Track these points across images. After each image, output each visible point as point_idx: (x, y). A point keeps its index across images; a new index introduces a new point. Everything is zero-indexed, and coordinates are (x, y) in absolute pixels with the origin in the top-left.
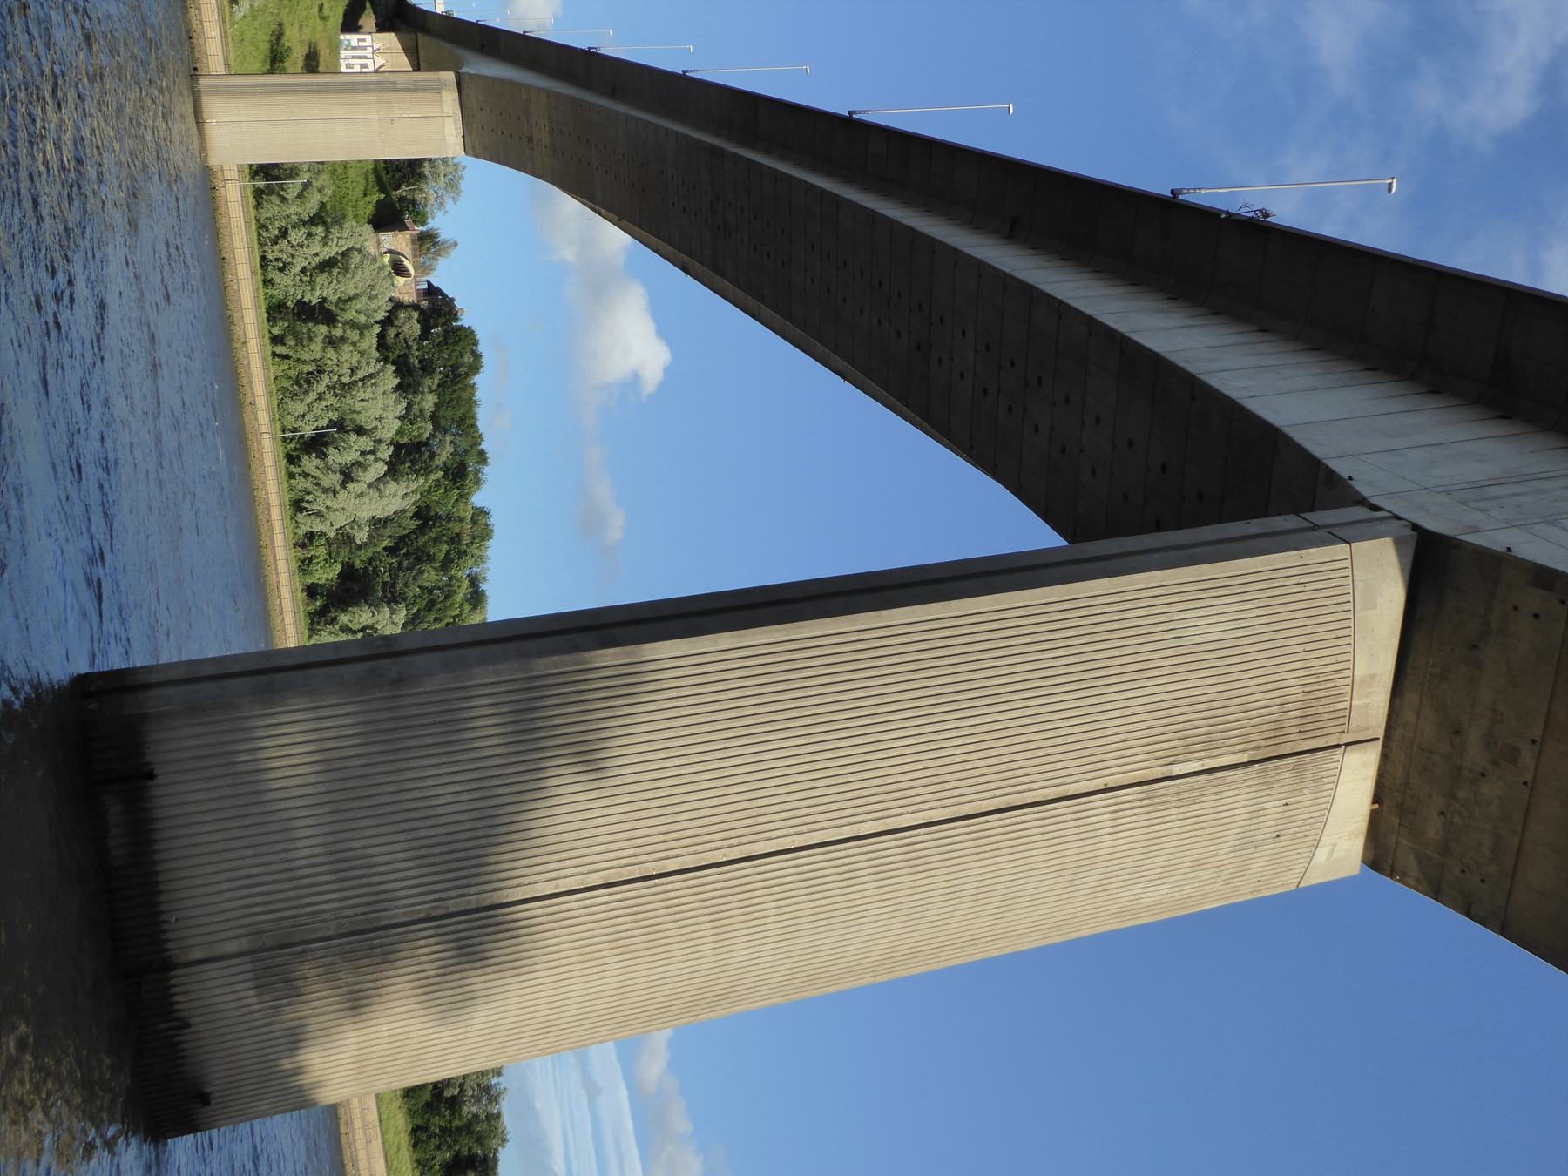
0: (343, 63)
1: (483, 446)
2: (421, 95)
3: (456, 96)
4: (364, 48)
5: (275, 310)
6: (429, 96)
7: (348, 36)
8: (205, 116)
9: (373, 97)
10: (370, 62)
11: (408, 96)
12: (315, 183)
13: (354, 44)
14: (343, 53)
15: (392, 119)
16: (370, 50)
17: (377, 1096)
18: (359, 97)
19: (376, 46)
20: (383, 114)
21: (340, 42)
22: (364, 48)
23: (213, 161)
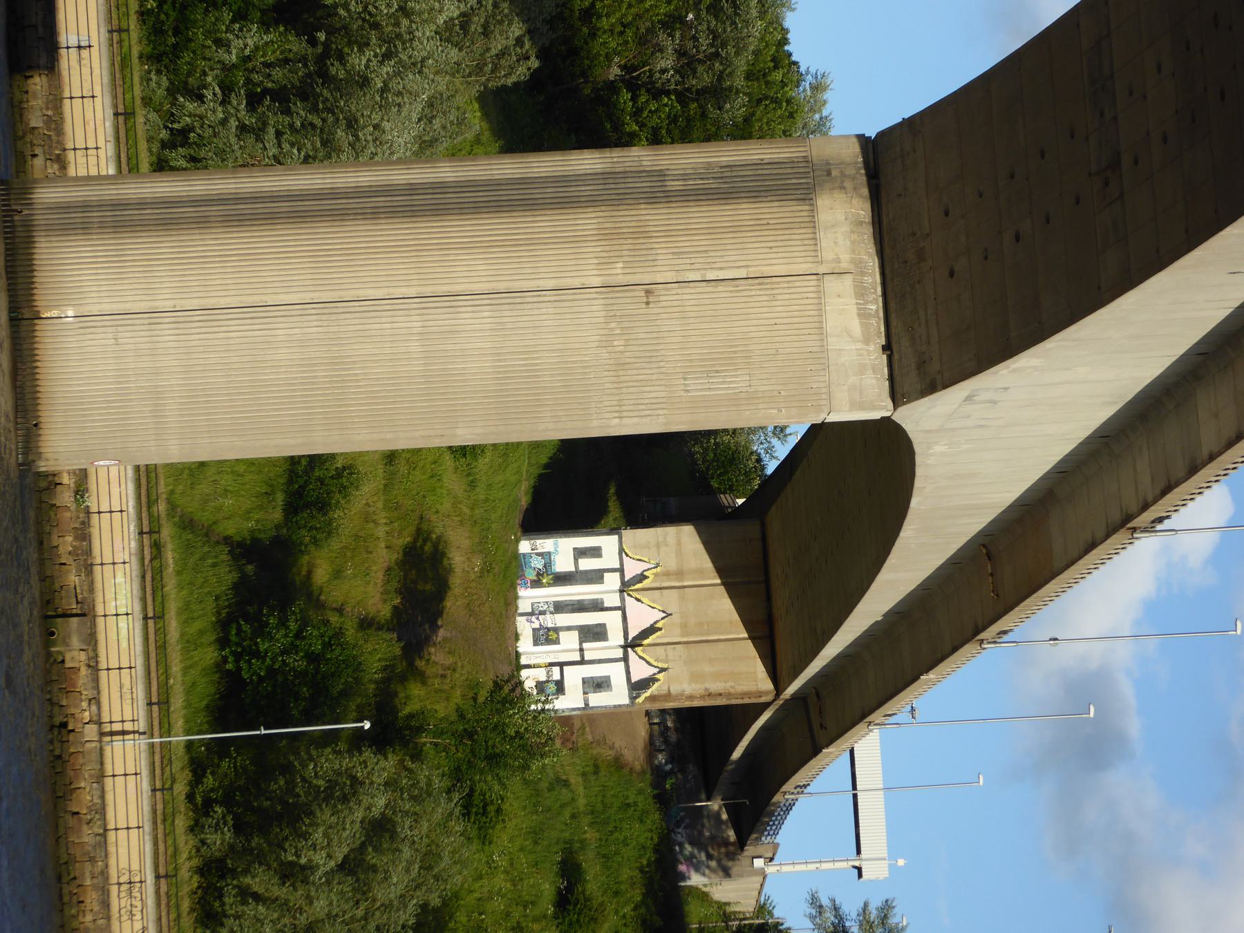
0: (525, 628)
1: (794, 58)
2: (745, 211)
3: (861, 208)
4: (596, 577)
5: (161, 166)
6: (771, 210)
7: (546, 544)
8: (42, 298)
9: (588, 221)
10: (612, 620)
11: (700, 215)
12: (404, 827)
13: (563, 563)
14: (528, 597)
15: (649, 291)
16: (613, 581)
17: (137, 468)
18: (544, 224)
19: (632, 569)
20: (618, 272)
21: (516, 563)
22: (596, 577)
23: (60, 449)
